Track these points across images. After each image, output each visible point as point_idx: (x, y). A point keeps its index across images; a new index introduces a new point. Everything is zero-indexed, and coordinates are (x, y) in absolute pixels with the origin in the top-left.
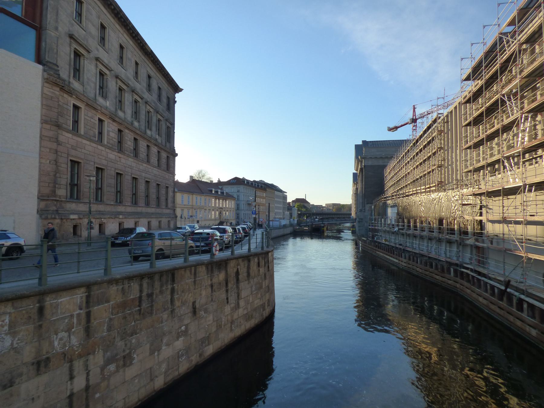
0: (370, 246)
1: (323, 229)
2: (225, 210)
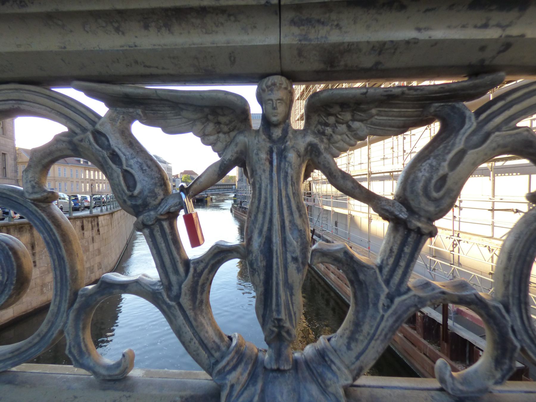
0: (239, 212)
1: (206, 199)
2: (97, 183)
